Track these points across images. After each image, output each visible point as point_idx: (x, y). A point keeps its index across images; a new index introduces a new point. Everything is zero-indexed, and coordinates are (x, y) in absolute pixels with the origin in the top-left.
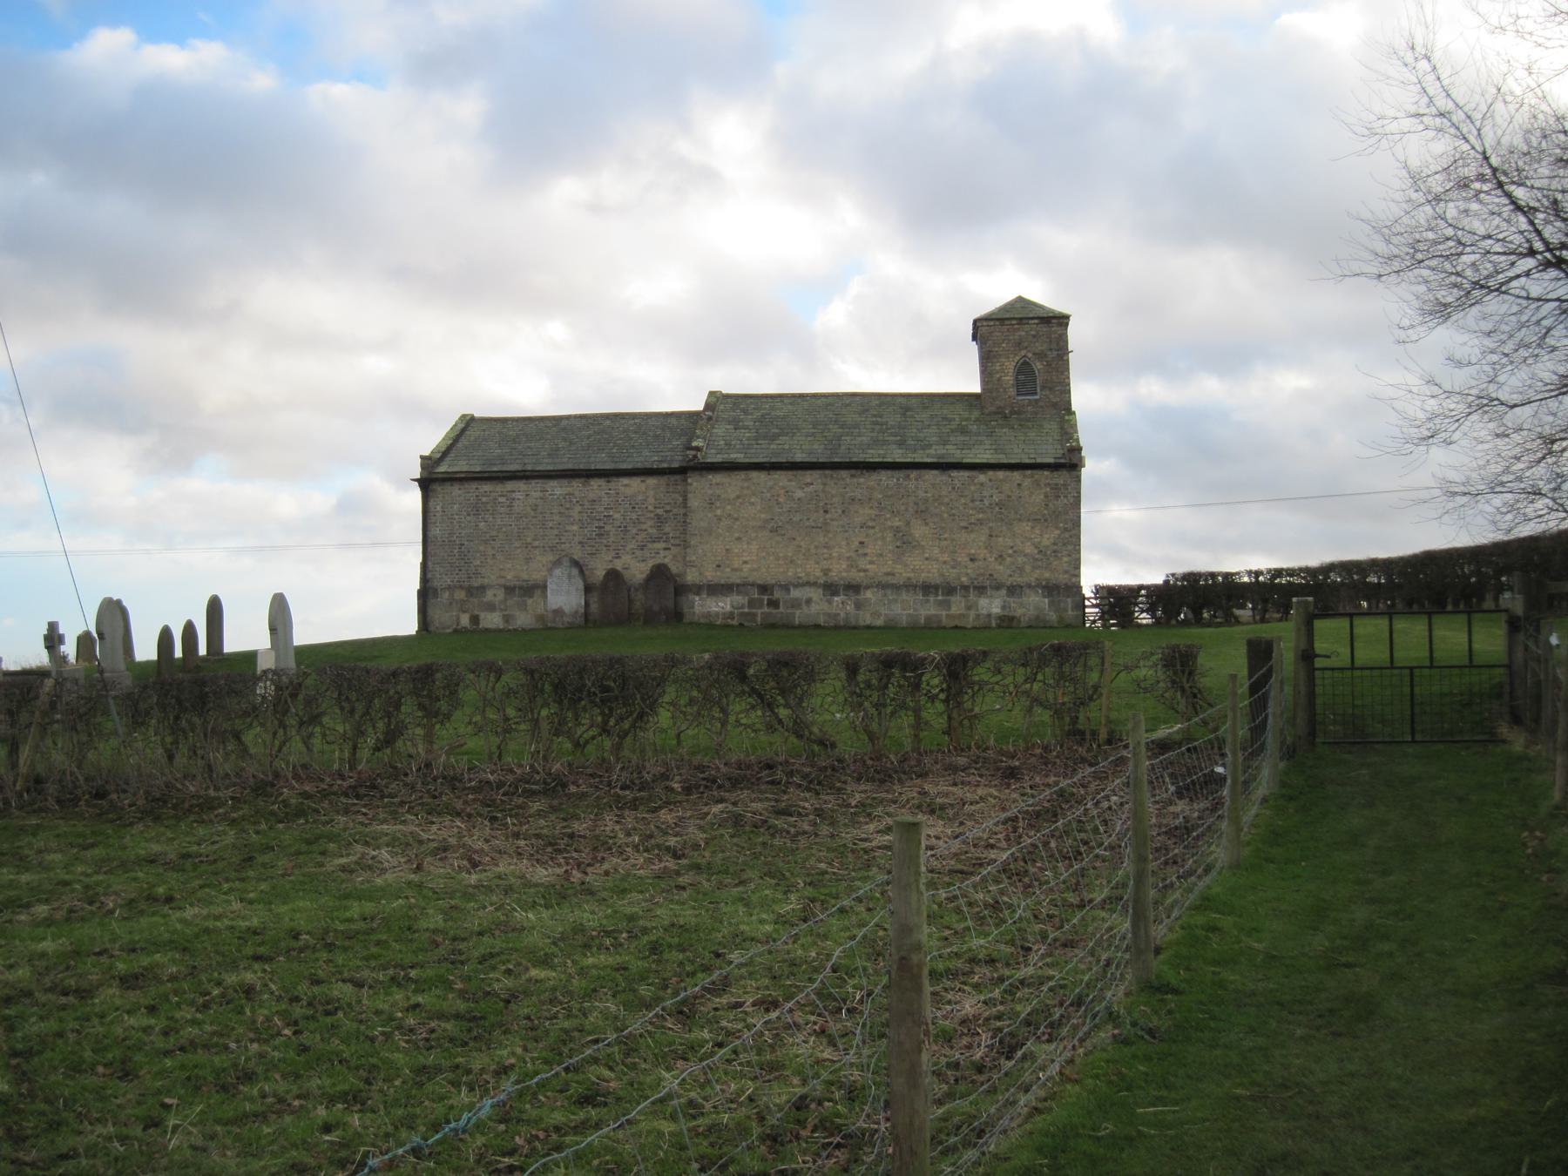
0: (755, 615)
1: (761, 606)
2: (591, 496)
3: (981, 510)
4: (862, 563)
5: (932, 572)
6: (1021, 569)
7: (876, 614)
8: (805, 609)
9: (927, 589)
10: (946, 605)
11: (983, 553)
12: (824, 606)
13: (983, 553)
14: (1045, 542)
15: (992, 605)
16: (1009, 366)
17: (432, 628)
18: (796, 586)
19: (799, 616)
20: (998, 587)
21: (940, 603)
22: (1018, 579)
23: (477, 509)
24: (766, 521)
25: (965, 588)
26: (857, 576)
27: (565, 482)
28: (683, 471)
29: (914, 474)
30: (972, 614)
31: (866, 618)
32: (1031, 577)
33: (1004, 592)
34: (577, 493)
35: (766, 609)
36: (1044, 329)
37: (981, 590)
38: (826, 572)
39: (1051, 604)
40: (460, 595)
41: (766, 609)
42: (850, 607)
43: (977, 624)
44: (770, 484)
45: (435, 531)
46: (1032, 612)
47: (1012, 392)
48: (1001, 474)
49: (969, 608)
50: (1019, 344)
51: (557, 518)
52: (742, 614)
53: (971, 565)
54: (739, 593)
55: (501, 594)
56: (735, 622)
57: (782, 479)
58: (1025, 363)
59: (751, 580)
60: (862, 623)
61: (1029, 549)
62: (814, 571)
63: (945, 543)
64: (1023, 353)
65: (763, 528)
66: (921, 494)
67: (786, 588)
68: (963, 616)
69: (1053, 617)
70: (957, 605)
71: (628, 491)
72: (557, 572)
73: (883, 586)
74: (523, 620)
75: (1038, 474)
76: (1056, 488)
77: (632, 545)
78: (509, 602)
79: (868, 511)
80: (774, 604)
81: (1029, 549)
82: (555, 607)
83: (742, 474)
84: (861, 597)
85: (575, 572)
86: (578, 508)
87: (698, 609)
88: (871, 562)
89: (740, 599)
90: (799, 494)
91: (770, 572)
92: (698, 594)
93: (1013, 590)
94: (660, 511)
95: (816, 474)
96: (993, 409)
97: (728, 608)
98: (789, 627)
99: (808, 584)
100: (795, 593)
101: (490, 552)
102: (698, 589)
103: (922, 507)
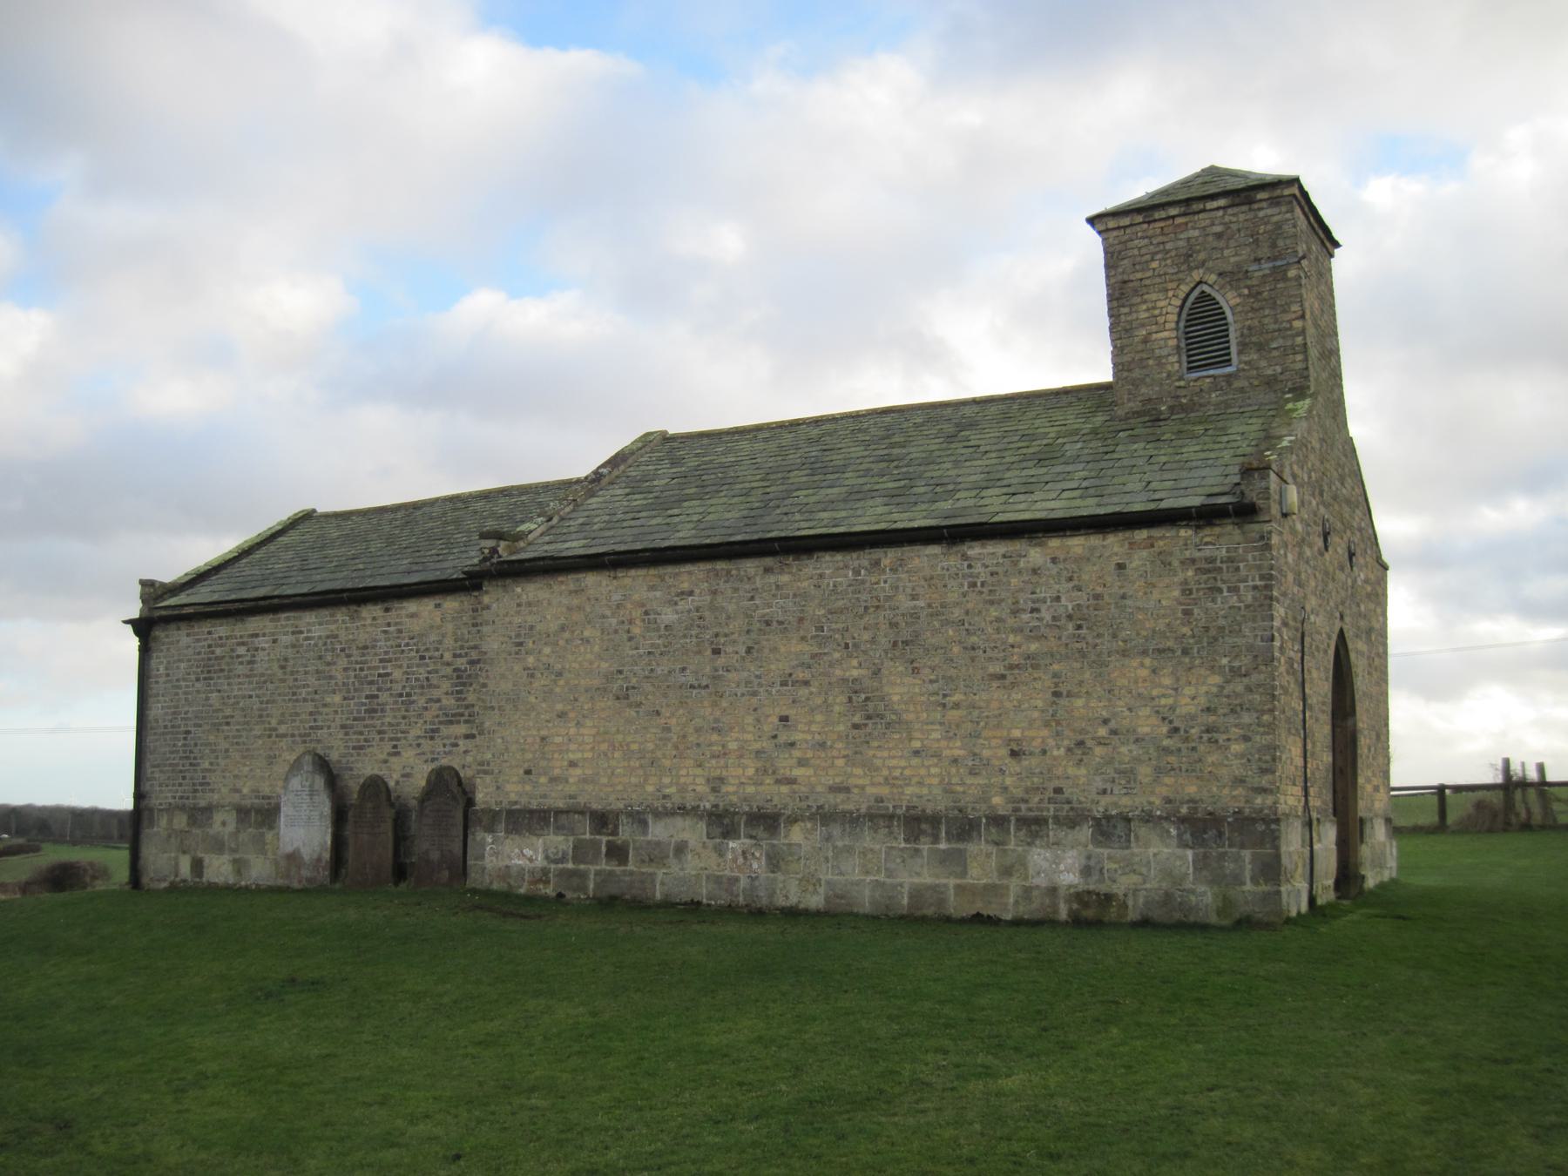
0: (583, 875)
1: (595, 861)
2: (363, 637)
3: (1035, 634)
4: (786, 764)
5: (925, 786)
6: (1129, 774)
7: (810, 881)
8: (674, 867)
9: (917, 823)
10: (956, 860)
11: (1039, 736)
12: (711, 861)
13: (1039, 736)
14: (1186, 706)
15: (1059, 866)
16: (1168, 307)
17: (145, 880)
18: (658, 815)
19: (667, 880)
20: (1072, 822)
21: (945, 859)
22: (1125, 802)
23: (210, 669)
24: (609, 677)
25: (999, 821)
26: (774, 795)
27: (325, 613)
28: (470, 583)
29: (888, 557)
30: (1014, 885)
31: (791, 892)
32: (1153, 798)
33: (1085, 832)
34: (343, 636)
35: (604, 866)
36: (1240, 216)
37: (1033, 826)
38: (716, 784)
39: (1201, 864)
40: (181, 821)
41: (604, 866)
42: (758, 865)
43: (1025, 911)
44: (616, 597)
45: (156, 711)
46: (1155, 883)
47: (1175, 364)
48: (1077, 544)
49: (1007, 871)
50: (1187, 258)
51: (312, 680)
52: (562, 874)
53: (1013, 766)
54: (559, 829)
55: (232, 818)
56: (550, 891)
57: (637, 584)
58: (1204, 297)
59: (582, 800)
60: (781, 902)
61: (1147, 724)
62: (692, 781)
63: (954, 715)
64: (1197, 275)
65: (603, 691)
66: (905, 603)
67: (639, 819)
68: (991, 890)
69: (1204, 898)
70: (981, 861)
71: (415, 626)
72: (295, 783)
73: (825, 817)
74: (260, 871)
75: (1165, 537)
76: (1209, 568)
77: (415, 732)
78: (243, 837)
79: (796, 647)
80: (618, 853)
81: (1147, 724)
82: (289, 849)
83: (569, 582)
84: (780, 842)
85: (320, 782)
86: (342, 662)
87: (490, 862)
88: (802, 763)
89: (560, 842)
90: (668, 616)
91: (614, 785)
92: (490, 829)
93: (1110, 828)
94: (461, 663)
95: (699, 570)
96: (1135, 405)
97: (540, 861)
98: (640, 906)
99: (683, 811)
100: (658, 831)
101: (224, 745)
102: (492, 819)
103: (906, 634)
